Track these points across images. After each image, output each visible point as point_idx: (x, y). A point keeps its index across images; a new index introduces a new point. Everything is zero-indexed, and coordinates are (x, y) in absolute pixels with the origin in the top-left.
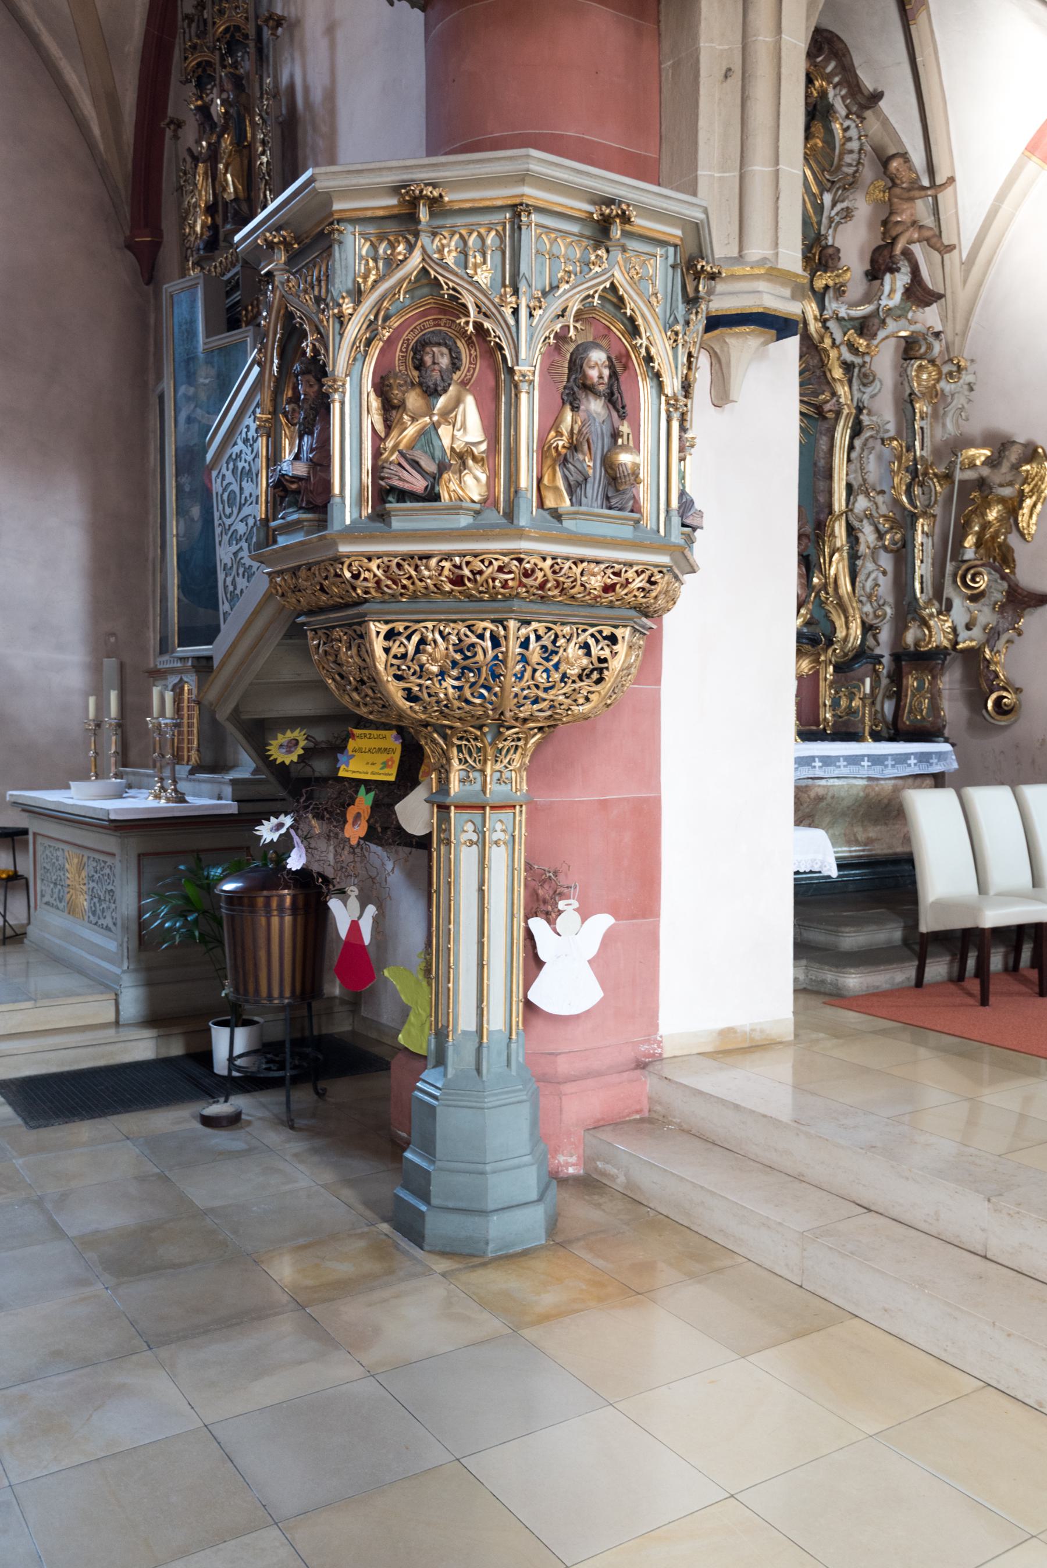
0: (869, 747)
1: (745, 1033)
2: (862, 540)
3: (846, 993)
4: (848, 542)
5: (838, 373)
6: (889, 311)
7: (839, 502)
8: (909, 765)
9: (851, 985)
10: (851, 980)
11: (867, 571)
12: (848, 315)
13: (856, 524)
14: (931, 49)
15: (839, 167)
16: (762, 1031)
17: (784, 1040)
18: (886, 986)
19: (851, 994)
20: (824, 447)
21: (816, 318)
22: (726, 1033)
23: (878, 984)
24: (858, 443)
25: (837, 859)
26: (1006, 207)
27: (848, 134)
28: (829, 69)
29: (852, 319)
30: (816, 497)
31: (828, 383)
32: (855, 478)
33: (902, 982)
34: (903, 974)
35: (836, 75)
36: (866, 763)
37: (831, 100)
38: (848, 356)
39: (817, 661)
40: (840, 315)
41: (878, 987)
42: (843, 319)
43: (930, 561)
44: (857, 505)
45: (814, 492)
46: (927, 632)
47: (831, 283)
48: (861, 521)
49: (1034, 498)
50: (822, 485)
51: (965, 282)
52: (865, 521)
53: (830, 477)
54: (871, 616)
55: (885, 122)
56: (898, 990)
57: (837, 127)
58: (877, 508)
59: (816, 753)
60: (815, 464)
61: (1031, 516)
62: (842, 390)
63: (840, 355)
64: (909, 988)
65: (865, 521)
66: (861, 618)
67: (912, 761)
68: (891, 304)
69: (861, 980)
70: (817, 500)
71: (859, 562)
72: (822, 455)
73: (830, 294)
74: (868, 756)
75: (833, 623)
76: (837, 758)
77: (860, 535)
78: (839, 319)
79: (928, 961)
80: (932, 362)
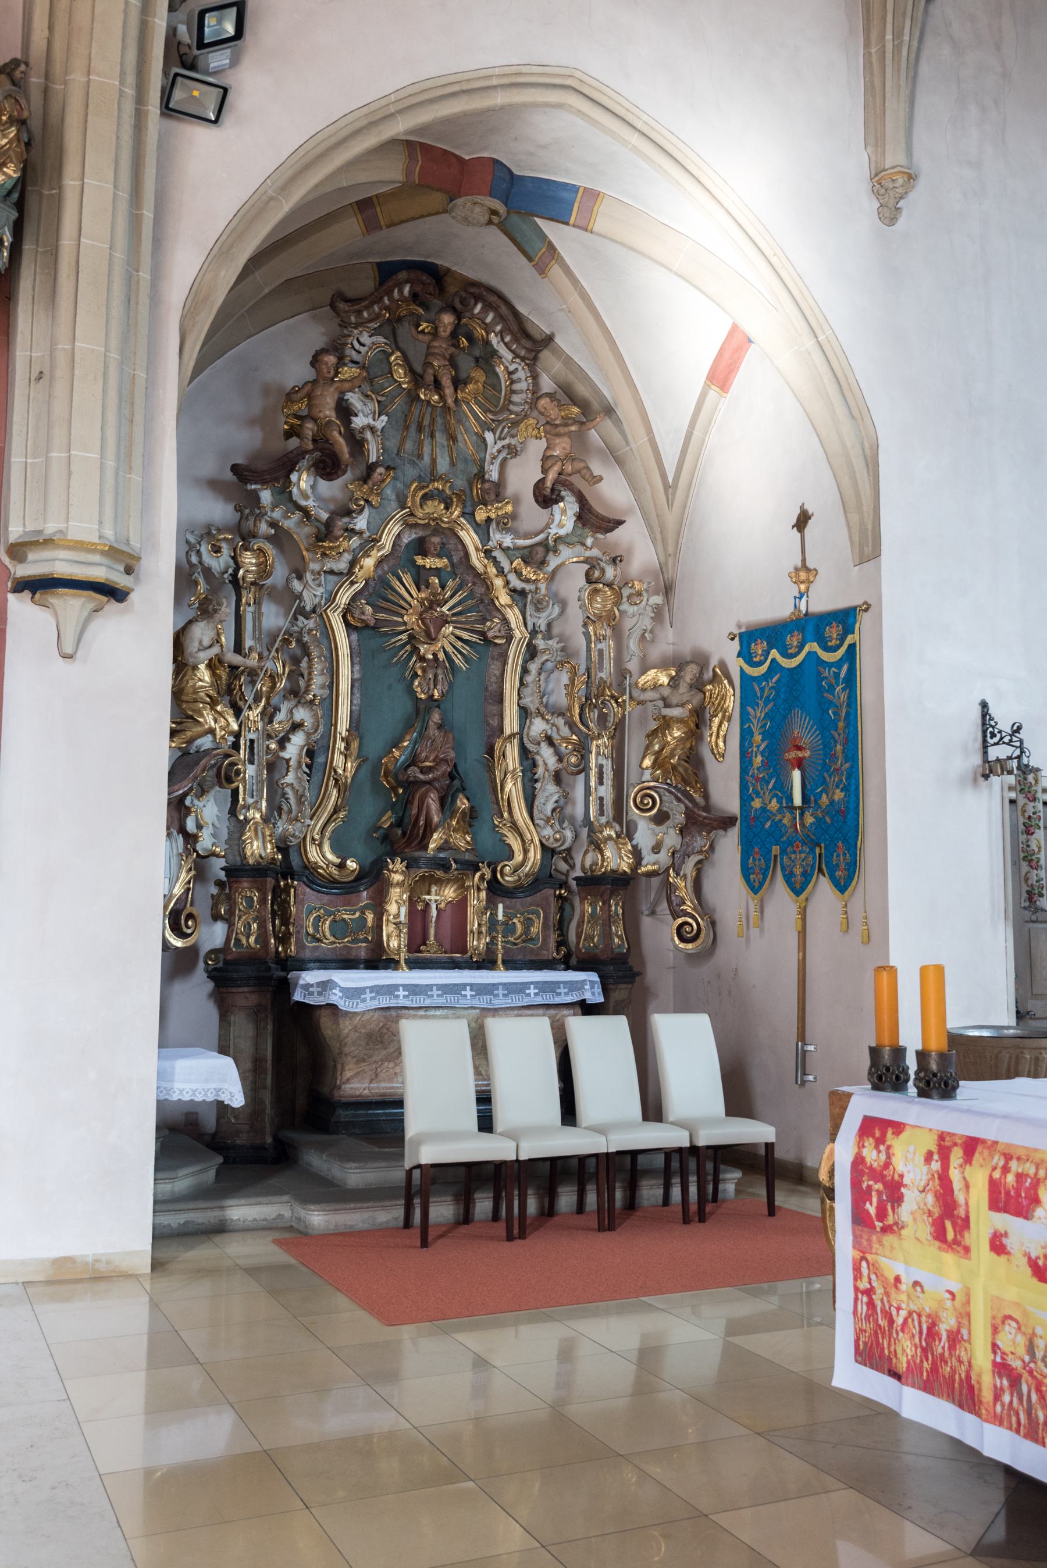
0: (500, 976)
1: (87, 1263)
2: (540, 762)
3: (311, 1232)
4: (521, 764)
5: (504, 598)
6: (558, 539)
7: (511, 723)
8: (529, 995)
9: (316, 1223)
10: (316, 1218)
11: (546, 794)
12: (514, 544)
13: (531, 747)
14: (574, 298)
15: (506, 408)
16: (108, 1262)
17: (137, 1272)
18: (361, 1226)
19: (316, 1232)
20: (496, 672)
21: (477, 549)
22: (61, 1262)
23: (353, 1223)
24: (533, 667)
25: (477, 1092)
26: (696, 433)
27: (515, 377)
28: (489, 320)
29: (517, 548)
30: (487, 721)
31: (498, 610)
32: (532, 702)
33: (387, 1222)
34: (390, 1214)
35: (498, 324)
36: (468, 992)
37: (495, 346)
38: (516, 583)
39: (462, 887)
40: (505, 545)
41: (351, 1226)
42: (508, 548)
43: (610, 783)
44: (533, 728)
45: (486, 716)
46: (599, 857)
47: (493, 516)
48: (539, 744)
49: (720, 715)
50: (493, 709)
51: (670, 503)
52: (543, 744)
53: (501, 700)
54: (552, 839)
55: (568, 361)
56: (379, 1230)
57: (500, 369)
58: (558, 730)
59: (400, 982)
60: (486, 689)
61: (718, 737)
62: (513, 616)
63: (508, 583)
64: (398, 1228)
65: (543, 744)
66: (541, 842)
67: (532, 991)
68: (562, 532)
69: (326, 1218)
70: (488, 724)
71: (538, 785)
72: (493, 679)
73: (493, 526)
74: (471, 985)
75: (509, 845)
76: (430, 987)
77: (537, 757)
78: (505, 550)
79: (431, 1199)
80: (610, 585)
